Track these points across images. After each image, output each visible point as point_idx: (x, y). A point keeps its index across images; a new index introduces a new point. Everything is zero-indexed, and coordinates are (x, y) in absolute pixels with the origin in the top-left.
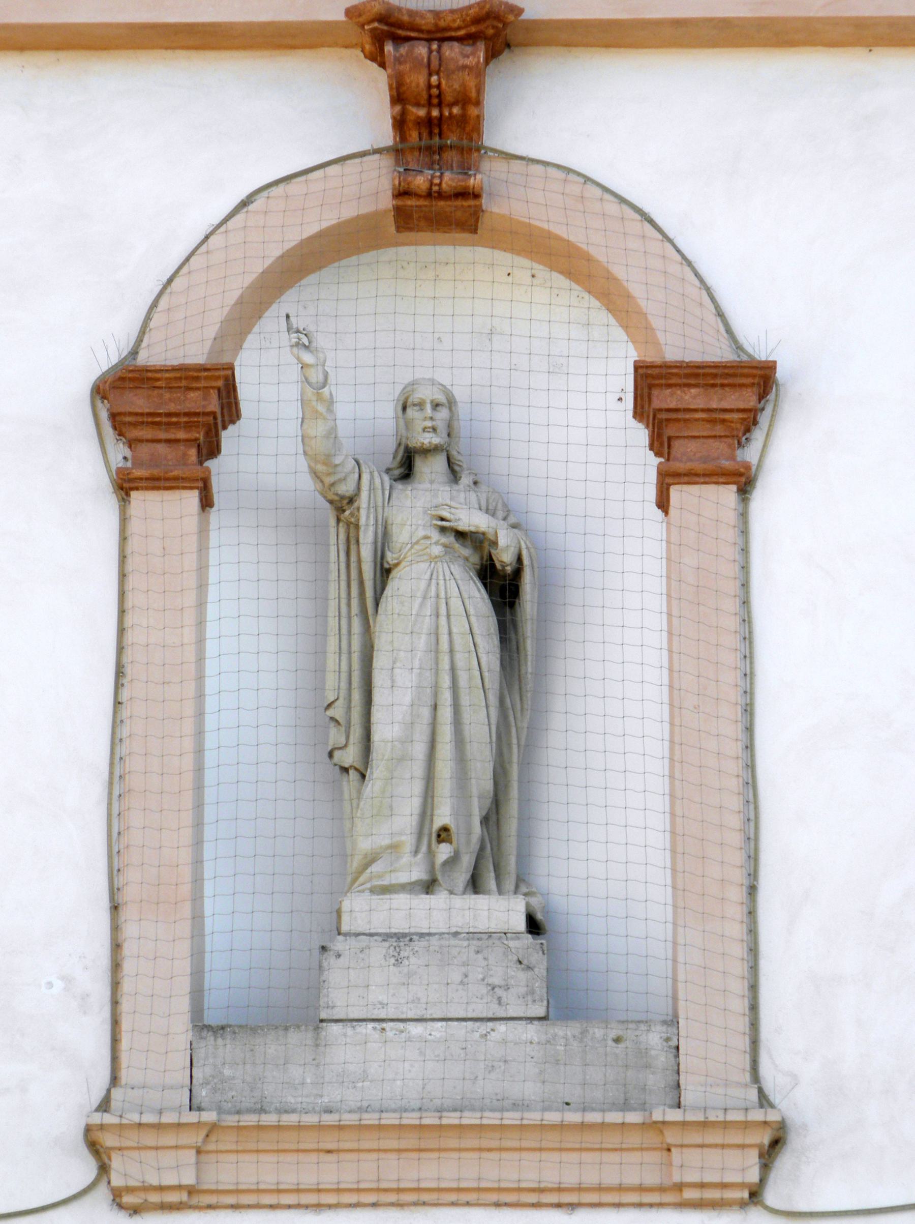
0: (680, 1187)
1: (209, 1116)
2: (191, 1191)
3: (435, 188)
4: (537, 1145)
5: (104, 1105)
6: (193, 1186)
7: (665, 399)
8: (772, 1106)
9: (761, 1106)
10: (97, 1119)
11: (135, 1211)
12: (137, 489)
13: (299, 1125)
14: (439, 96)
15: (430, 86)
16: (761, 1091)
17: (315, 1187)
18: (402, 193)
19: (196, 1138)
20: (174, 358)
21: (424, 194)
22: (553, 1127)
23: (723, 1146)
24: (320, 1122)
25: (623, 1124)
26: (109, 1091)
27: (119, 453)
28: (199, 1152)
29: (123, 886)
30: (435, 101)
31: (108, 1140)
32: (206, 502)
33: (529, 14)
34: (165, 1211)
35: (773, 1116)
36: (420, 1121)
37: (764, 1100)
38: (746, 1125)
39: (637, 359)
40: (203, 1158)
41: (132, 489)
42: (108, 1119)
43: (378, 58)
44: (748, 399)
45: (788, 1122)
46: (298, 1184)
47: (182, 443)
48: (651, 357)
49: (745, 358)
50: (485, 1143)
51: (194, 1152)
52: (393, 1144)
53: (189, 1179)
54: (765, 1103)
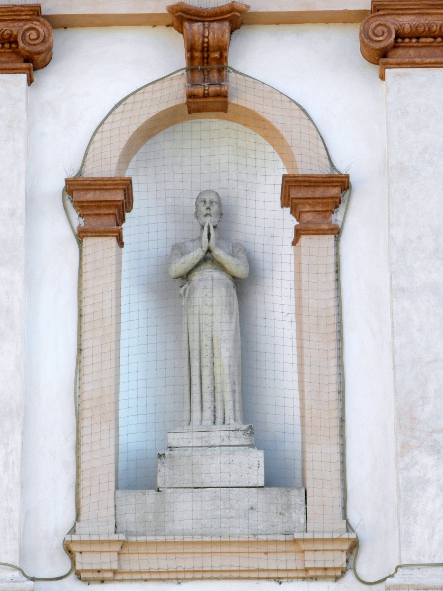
0: (306, 570)
1: (122, 537)
2: (115, 572)
3: (206, 92)
4: (155, 551)
5: (73, 531)
6: (117, 570)
7: (294, 193)
8: (353, 531)
9: (348, 531)
10: (68, 538)
11: (87, 581)
12: (87, 236)
13: (165, 542)
14: (208, 47)
15: (203, 42)
16: (347, 523)
17: (148, 571)
18: (191, 96)
19: (117, 548)
20: (97, 174)
21: (202, 96)
22: (151, 543)
23: (101, 552)
24: (165, 540)
25: (286, 541)
26: (75, 524)
27: (77, 221)
28: (119, 554)
29: (81, 428)
30: (206, 49)
31: (75, 548)
32: (121, 243)
33: (253, 9)
34: (203, 580)
35: (353, 536)
36: (193, 539)
37: (349, 528)
38: (109, 542)
39: (286, 172)
40: (122, 557)
41: (84, 236)
42: (75, 538)
43: (180, 30)
44: (119, 196)
45: (360, 539)
46: (149, 569)
47: (111, 215)
48: (291, 172)
49: (336, 173)
50: (251, 550)
51: (116, 554)
52: (246, 550)
53: (115, 566)
54: (350, 530)
